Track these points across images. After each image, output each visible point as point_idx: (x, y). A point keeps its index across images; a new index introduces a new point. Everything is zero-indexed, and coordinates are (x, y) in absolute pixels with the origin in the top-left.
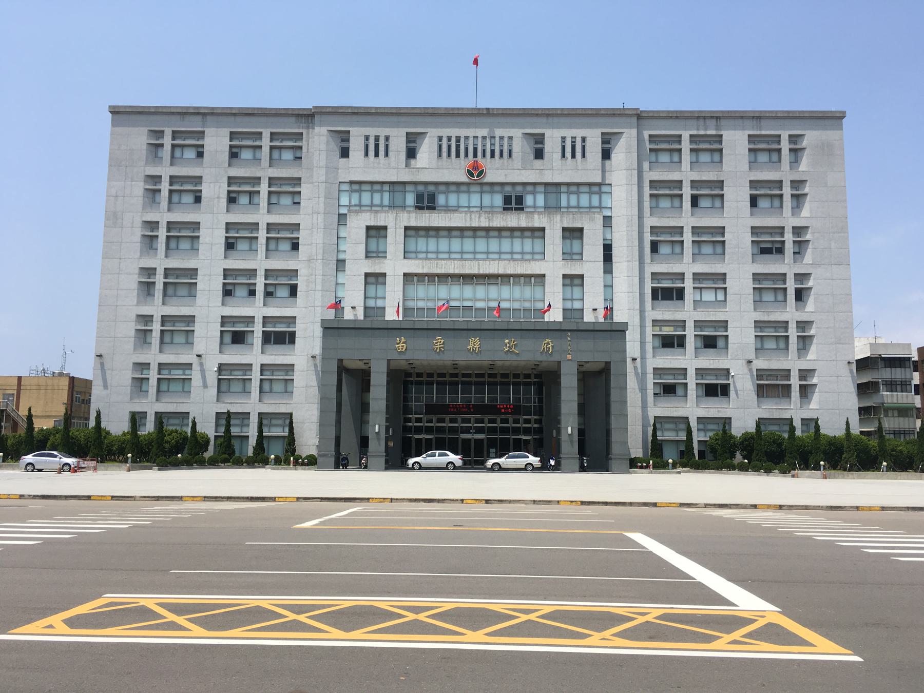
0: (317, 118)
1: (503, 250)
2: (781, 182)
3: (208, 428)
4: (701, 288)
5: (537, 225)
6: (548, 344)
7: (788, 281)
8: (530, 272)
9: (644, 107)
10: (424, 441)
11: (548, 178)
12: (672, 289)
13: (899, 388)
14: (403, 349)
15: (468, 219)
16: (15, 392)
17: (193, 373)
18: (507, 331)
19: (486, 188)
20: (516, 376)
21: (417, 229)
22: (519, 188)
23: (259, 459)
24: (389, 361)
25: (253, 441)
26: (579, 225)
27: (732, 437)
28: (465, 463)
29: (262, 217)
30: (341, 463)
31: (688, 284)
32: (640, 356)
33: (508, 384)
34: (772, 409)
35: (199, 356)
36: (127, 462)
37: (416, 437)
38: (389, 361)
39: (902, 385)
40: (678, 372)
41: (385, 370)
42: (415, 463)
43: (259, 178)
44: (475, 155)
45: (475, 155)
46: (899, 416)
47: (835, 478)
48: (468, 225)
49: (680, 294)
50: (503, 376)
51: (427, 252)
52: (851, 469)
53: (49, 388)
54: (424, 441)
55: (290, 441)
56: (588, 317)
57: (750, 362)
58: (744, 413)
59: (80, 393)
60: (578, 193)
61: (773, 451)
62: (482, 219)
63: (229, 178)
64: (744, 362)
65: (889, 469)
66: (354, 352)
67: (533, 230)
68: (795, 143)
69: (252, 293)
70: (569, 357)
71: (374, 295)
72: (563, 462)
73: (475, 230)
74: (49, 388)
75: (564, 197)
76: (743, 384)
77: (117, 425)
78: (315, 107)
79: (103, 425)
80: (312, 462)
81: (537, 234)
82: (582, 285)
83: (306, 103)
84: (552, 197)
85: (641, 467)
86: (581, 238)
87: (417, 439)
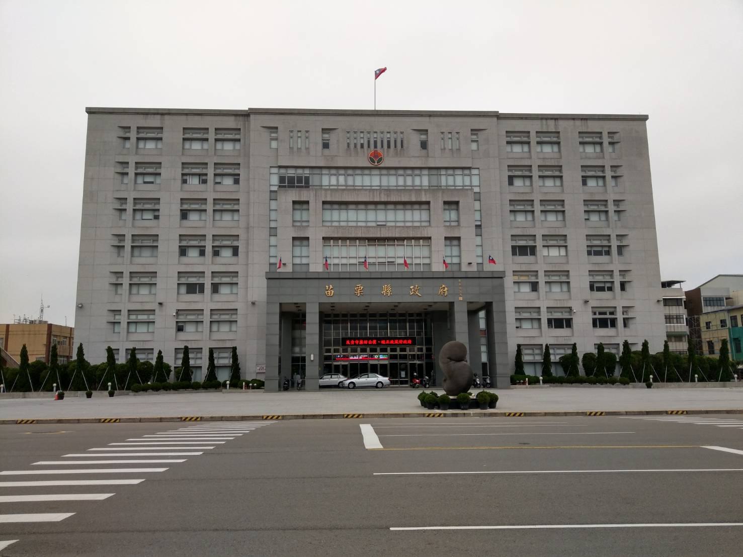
0: (252, 117)
1: (389, 219)
2: (603, 167)
3: (172, 361)
4: (548, 246)
5: (424, 199)
6: (444, 288)
7: (612, 240)
8: (419, 236)
9: (502, 111)
10: (341, 367)
11: (432, 164)
12: (526, 247)
13: (675, 320)
14: (332, 294)
15: (371, 196)
16: (4, 337)
17: (239, 316)
18: (412, 278)
19: (384, 172)
20: (411, 315)
21: (331, 203)
22: (307, 171)
23: (212, 384)
24: (281, 304)
25: (205, 371)
26: (456, 199)
27: (96, 367)
28: (392, 382)
29: (209, 193)
30: (287, 386)
31: (539, 243)
32: (515, 297)
33: (405, 321)
34: (604, 334)
35: (160, 304)
36: (52, 390)
37: (335, 363)
38: (281, 304)
39: (677, 318)
40: (534, 310)
41: (318, 311)
42: (350, 383)
43: (206, 164)
44: (376, 147)
45: (376, 147)
46: (675, 341)
47: (662, 387)
48: (371, 200)
49: (532, 250)
50: (401, 315)
51: (332, 221)
52: (670, 380)
53: (32, 333)
54: (341, 367)
55: (235, 368)
56: (464, 268)
57: (586, 302)
58: (586, 339)
59: (56, 336)
60: (337, 175)
61: (600, 369)
62: (382, 195)
63: (183, 164)
64: (581, 302)
65: (700, 380)
66: (292, 295)
67: (420, 203)
68: (612, 138)
69: (202, 253)
70: (461, 299)
71: (299, 255)
72: (307, 382)
73: (376, 203)
74: (32, 333)
75: (443, 178)
76: (583, 319)
77: (96, 357)
78: (250, 109)
79: (85, 357)
80: (259, 385)
81: (424, 207)
82: (459, 245)
83: (244, 107)
84: (434, 178)
85: (520, 383)
86: (457, 209)
87: (335, 366)
